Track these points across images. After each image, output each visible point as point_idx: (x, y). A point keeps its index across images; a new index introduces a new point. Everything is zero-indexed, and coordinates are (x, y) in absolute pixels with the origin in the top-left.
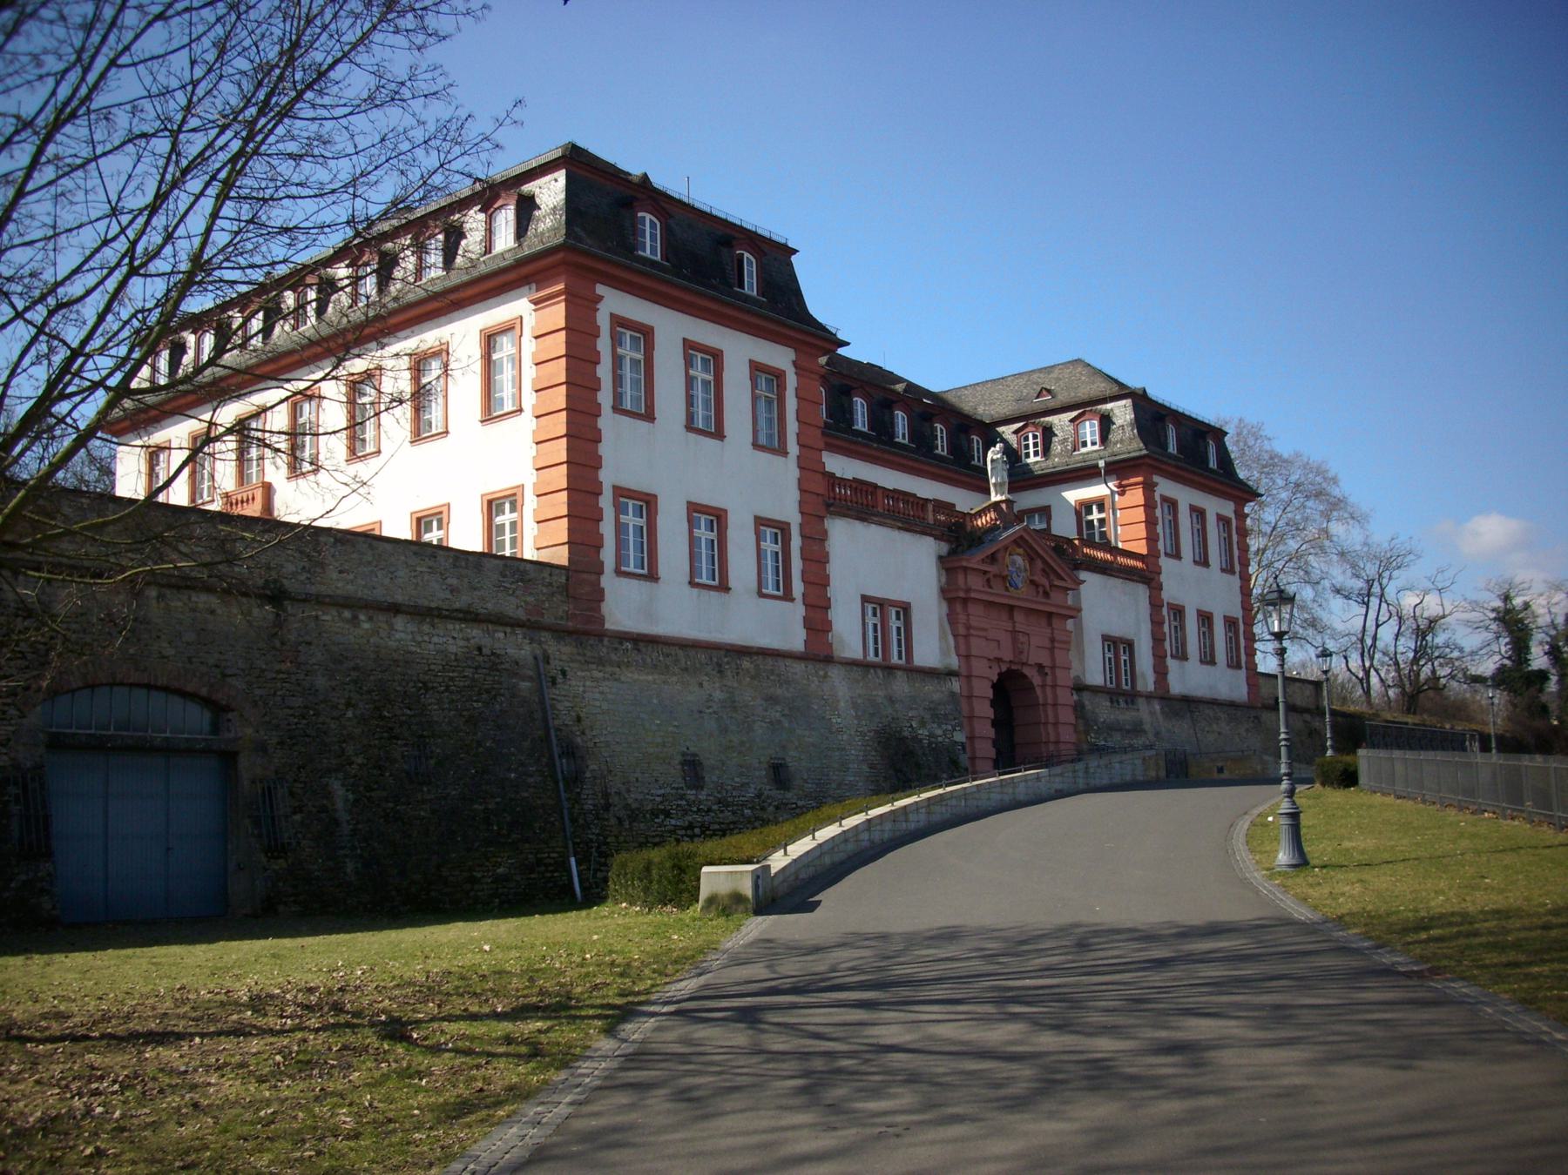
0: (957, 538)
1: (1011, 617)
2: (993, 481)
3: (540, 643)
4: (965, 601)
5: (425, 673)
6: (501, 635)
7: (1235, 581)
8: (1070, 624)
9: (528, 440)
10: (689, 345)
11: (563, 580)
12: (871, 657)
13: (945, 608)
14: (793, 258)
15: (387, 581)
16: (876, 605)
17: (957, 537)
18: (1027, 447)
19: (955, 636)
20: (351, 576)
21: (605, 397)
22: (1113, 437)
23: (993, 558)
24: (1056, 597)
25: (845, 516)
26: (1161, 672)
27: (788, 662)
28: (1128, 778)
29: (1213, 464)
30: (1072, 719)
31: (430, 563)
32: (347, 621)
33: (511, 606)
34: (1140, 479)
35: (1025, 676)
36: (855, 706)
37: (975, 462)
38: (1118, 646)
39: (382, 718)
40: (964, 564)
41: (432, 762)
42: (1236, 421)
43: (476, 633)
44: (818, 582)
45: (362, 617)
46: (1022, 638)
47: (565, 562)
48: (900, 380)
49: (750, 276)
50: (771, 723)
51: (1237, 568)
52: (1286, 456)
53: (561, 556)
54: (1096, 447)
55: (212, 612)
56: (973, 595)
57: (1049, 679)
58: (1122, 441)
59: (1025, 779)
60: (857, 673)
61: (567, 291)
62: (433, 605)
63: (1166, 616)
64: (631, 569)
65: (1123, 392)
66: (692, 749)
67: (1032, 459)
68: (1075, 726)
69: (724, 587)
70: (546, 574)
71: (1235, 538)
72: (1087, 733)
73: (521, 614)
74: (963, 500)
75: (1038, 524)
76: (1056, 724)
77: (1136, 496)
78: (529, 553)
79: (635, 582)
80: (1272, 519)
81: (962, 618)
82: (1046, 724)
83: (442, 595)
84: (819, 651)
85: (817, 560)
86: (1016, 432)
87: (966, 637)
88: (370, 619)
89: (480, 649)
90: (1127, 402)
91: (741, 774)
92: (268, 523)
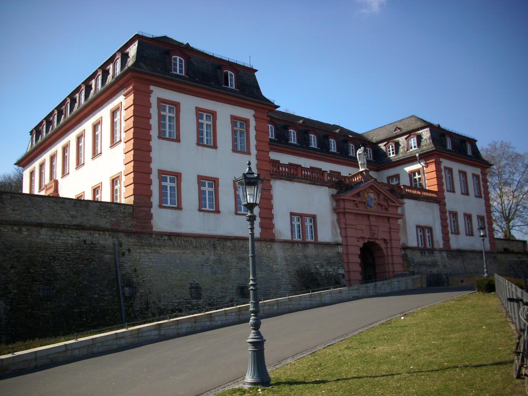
0: (340, 187)
1: (369, 219)
2: (360, 163)
3: (118, 238)
4: (344, 213)
5: (55, 253)
6: (97, 235)
7: (482, 201)
8: (400, 221)
9: (122, 152)
10: (198, 109)
11: (131, 210)
12: (296, 239)
13: (335, 217)
14: (256, 74)
15: (38, 214)
16: (421, 228)
17: (340, 186)
18: (389, 151)
19: (340, 228)
20: (19, 212)
21: (154, 133)
22: (423, 144)
23: (358, 195)
24: (391, 210)
25: (281, 179)
26: (446, 239)
28: (403, 288)
29: (469, 153)
30: (401, 261)
31: (61, 205)
32: (16, 231)
33: (103, 223)
34: (434, 160)
35: (378, 245)
36: (286, 260)
37: (351, 155)
38: (424, 230)
39: (29, 272)
40: (342, 197)
41: (54, 291)
42: (500, 142)
43: (84, 235)
45: (24, 229)
46: (374, 228)
47: (132, 203)
48: (300, 118)
49: (231, 80)
50: (240, 269)
51: (483, 195)
52: (522, 154)
54: (416, 149)
56: (347, 210)
57: (389, 245)
58: (426, 145)
59: (331, 293)
60: (288, 246)
61: (134, 88)
62: (61, 223)
63: (448, 218)
64: (207, 208)
65: (428, 125)
66: (196, 282)
67: (392, 156)
68: (403, 264)
69: (218, 211)
70: (122, 208)
71: (481, 183)
72: (408, 267)
73: (108, 226)
74: (345, 171)
75: (395, 183)
76: (393, 264)
77: (432, 167)
79: (169, 211)
80: (518, 179)
81: (343, 220)
82: (388, 264)
83: (67, 219)
84: (268, 236)
86: (385, 145)
87: (345, 228)
88: (28, 230)
89: (85, 241)
90: (428, 129)
91: (222, 292)
92: (55, 199)
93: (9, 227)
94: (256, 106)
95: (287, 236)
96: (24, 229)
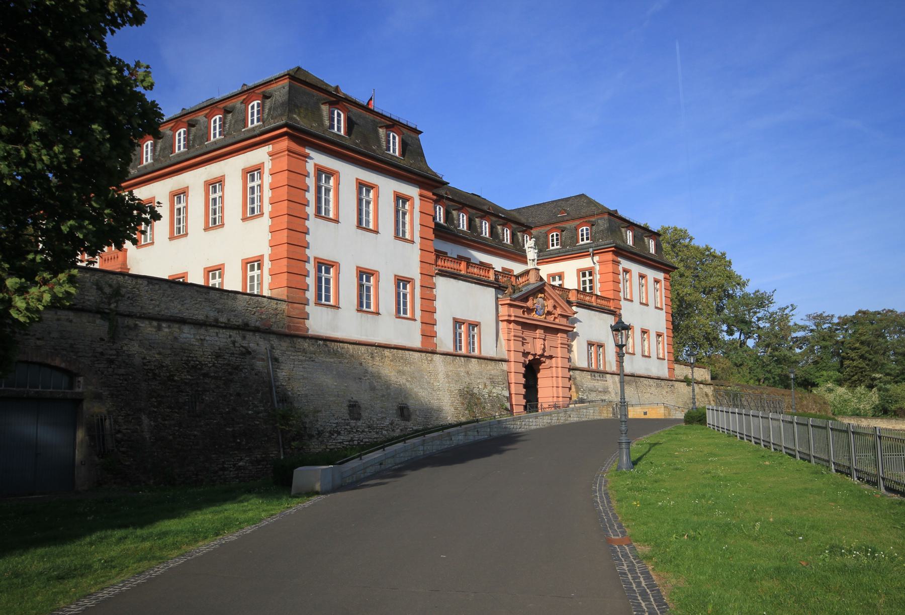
27: (411, 353)
36: (448, 376)
38: (595, 346)
44: (429, 311)
55: (71, 321)
66: (355, 399)
75: (557, 283)
78: (266, 292)
85: (429, 299)
88: (169, 327)
91: (382, 412)
93: (147, 322)
94: (423, 183)
95: (449, 347)
96: (164, 325)
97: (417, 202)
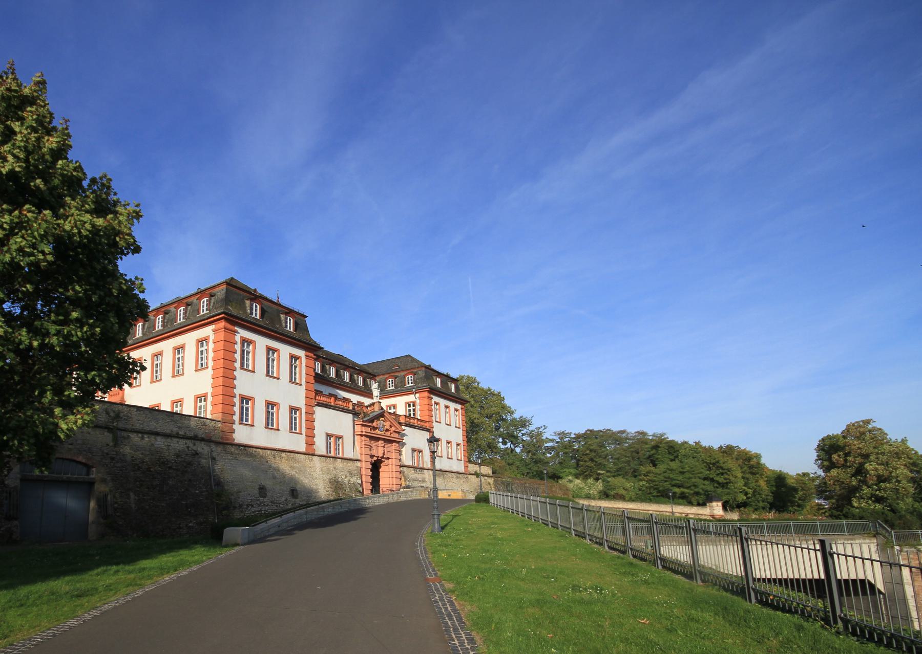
36: (322, 470)
44: (311, 428)
53: (218, 417)
85: (310, 421)
97: (304, 360)
